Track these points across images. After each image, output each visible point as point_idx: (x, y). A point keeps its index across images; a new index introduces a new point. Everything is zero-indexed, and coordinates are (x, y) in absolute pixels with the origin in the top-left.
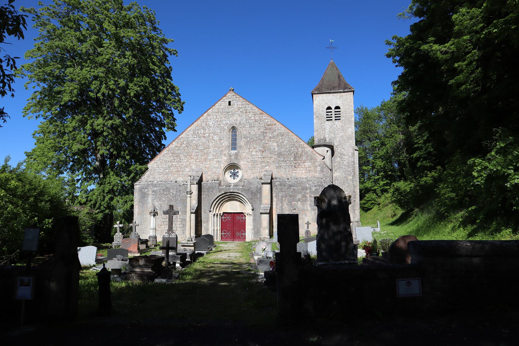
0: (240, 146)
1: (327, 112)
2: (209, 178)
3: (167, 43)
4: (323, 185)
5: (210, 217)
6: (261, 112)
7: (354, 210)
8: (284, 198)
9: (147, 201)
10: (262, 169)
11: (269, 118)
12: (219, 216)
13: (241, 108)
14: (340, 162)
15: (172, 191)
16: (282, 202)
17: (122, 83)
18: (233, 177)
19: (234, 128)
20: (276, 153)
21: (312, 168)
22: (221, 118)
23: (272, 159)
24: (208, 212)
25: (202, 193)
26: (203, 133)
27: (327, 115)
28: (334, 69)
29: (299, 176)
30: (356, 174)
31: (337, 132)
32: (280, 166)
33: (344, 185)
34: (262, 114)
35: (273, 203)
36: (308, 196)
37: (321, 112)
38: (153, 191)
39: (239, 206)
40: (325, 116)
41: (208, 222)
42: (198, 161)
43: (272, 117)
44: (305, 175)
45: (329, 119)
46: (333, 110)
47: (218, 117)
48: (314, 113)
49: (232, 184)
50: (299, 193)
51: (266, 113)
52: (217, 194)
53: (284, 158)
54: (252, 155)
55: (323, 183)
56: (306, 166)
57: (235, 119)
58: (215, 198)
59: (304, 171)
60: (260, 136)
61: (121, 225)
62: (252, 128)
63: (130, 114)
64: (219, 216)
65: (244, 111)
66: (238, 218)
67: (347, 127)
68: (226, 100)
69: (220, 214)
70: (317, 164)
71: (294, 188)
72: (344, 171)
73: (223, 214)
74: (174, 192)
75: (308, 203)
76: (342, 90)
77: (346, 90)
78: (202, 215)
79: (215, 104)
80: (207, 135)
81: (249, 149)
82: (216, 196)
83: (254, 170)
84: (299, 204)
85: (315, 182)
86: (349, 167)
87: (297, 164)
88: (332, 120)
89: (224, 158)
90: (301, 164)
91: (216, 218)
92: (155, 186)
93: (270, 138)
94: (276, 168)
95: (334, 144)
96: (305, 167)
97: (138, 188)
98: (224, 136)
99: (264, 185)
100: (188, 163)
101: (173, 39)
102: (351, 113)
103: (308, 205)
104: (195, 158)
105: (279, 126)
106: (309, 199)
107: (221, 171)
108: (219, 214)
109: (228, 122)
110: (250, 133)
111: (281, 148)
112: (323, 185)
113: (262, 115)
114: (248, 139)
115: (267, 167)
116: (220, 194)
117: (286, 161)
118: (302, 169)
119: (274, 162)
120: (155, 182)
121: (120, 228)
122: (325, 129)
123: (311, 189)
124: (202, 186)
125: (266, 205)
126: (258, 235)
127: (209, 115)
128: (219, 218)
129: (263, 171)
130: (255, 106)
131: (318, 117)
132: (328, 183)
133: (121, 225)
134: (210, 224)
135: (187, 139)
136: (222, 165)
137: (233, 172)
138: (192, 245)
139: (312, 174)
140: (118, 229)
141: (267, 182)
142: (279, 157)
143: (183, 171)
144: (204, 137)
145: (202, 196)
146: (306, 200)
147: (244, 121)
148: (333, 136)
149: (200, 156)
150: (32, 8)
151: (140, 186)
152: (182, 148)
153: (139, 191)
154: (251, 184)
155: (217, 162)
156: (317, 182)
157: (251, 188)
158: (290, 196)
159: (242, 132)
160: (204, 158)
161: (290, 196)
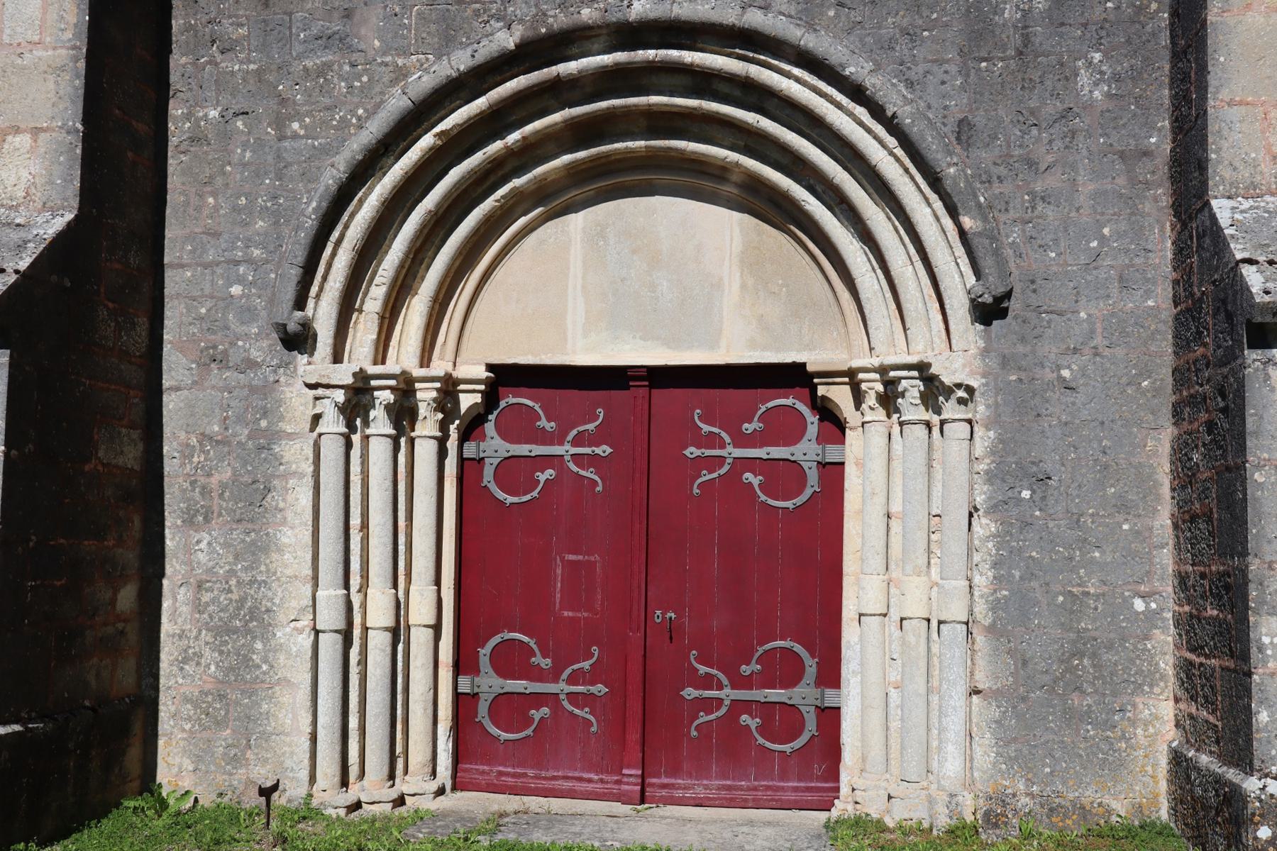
12: (427, 425)
24: (264, 348)
25: (179, 61)
39: (732, 280)
52: (401, 74)
58: (375, 129)
64: (427, 425)
69: (449, 388)
73: (491, 397)
78: (171, 403)
82: (397, 103)
91: (380, 451)
108: (426, 395)
116: (461, 61)
126: (1072, 717)
128: (425, 452)
138: (417, 385)
145: (176, 110)
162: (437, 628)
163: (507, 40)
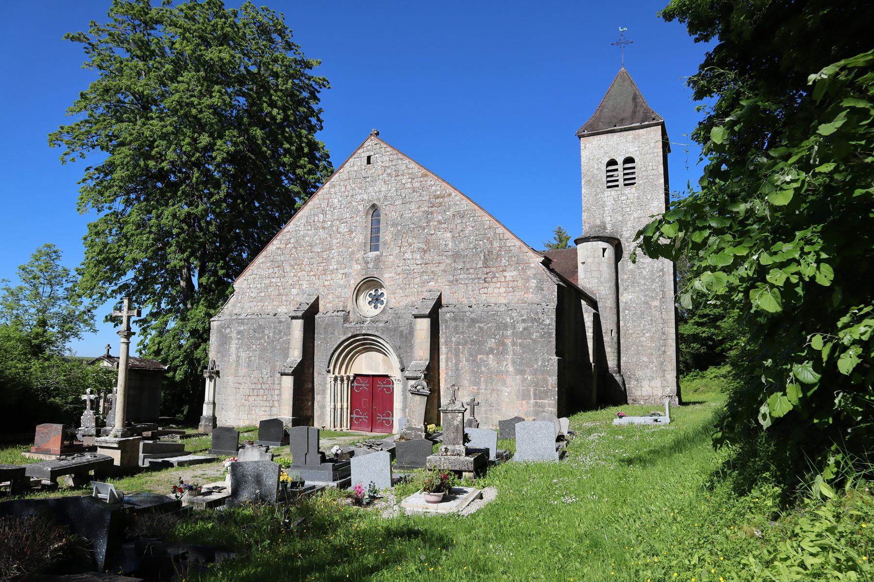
0: (384, 242)
1: (608, 171)
2: (329, 306)
3: (311, 68)
4: (540, 319)
5: (328, 382)
6: (424, 171)
7: (664, 371)
8: (461, 347)
9: (229, 351)
10: (422, 287)
11: (438, 183)
12: (346, 382)
13: (388, 167)
14: (635, 272)
15: (267, 332)
16: (457, 355)
17: (204, 139)
18: (373, 305)
19: (374, 206)
20: (450, 253)
21: (520, 283)
22: (353, 189)
23: (442, 267)
24: (325, 372)
26: (321, 220)
27: (608, 177)
28: (627, 83)
29: (493, 300)
30: (667, 296)
31: (628, 210)
32: (457, 280)
33: (643, 318)
34: (426, 175)
35: (441, 357)
36: (508, 342)
37: (596, 172)
38: (239, 333)
39: (381, 363)
40: (605, 180)
41: (324, 391)
42: (312, 273)
43: (444, 181)
44: (505, 297)
45: (612, 184)
46: (620, 167)
47: (349, 188)
48: (582, 175)
49: (368, 319)
50: (490, 337)
51: (433, 173)
53: (464, 262)
54: (405, 260)
55: (540, 315)
56: (507, 280)
57: (376, 191)
58: (335, 346)
59: (502, 290)
60: (421, 220)
61: (92, 397)
62: (408, 205)
63: (222, 194)
64: (346, 382)
65: (394, 173)
66: (380, 385)
67: (649, 198)
68: (363, 154)
69: (348, 377)
70: (530, 273)
71: (482, 325)
72: (642, 290)
74: (271, 335)
75: (509, 357)
76: (638, 124)
77: (646, 123)
78: (315, 379)
79: (344, 164)
80: (329, 223)
81: (400, 247)
83: (407, 290)
84: (491, 359)
85: (523, 312)
86: (653, 281)
87: (490, 275)
88: (617, 186)
89: (356, 268)
90: (497, 275)
92: (242, 322)
93: (439, 222)
94: (448, 284)
95: (621, 236)
96: (505, 281)
97: (215, 327)
98: (357, 224)
99: (418, 320)
100: (296, 279)
101: (319, 60)
102: (657, 169)
103: (510, 361)
104: (307, 268)
105: (457, 198)
106: (510, 348)
107: (349, 292)
109: (366, 197)
110: (403, 214)
111: (459, 243)
112: (540, 319)
113: (426, 179)
114: (399, 228)
115: (431, 283)
117: (468, 269)
118: (498, 285)
119: (444, 271)
120: (244, 315)
121: (91, 401)
122: (603, 206)
123: (515, 328)
124: (316, 322)
125: (422, 362)
127: (334, 186)
128: (346, 386)
129: (425, 290)
130: (413, 160)
131: (589, 181)
132: (550, 314)
133: (92, 397)
134: (328, 396)
135: (297, 234)
136: (352, 282)
137: (374, 294)
138: (116, 446)
139: (519, 294)
140: (88, 403)
141: (423, 313)
142: (455, 262)
143: (287, 295)
144: (324, 228)
146: (504, 352)
147: (392, 193)
148: (620, 218)
149: (315, 265)
150: (80, 32)
151: (219, 322)
152: (287, 251)
153: (217, 333)
154: (399, 318)
155: (344, 276)
156: (528, 313)
157: (399, 327)
158: (473, 342)
159: (388, 213)
160: (322, 268)
161: (473, 342)
162: (347, 408)
163: (350, 335)
